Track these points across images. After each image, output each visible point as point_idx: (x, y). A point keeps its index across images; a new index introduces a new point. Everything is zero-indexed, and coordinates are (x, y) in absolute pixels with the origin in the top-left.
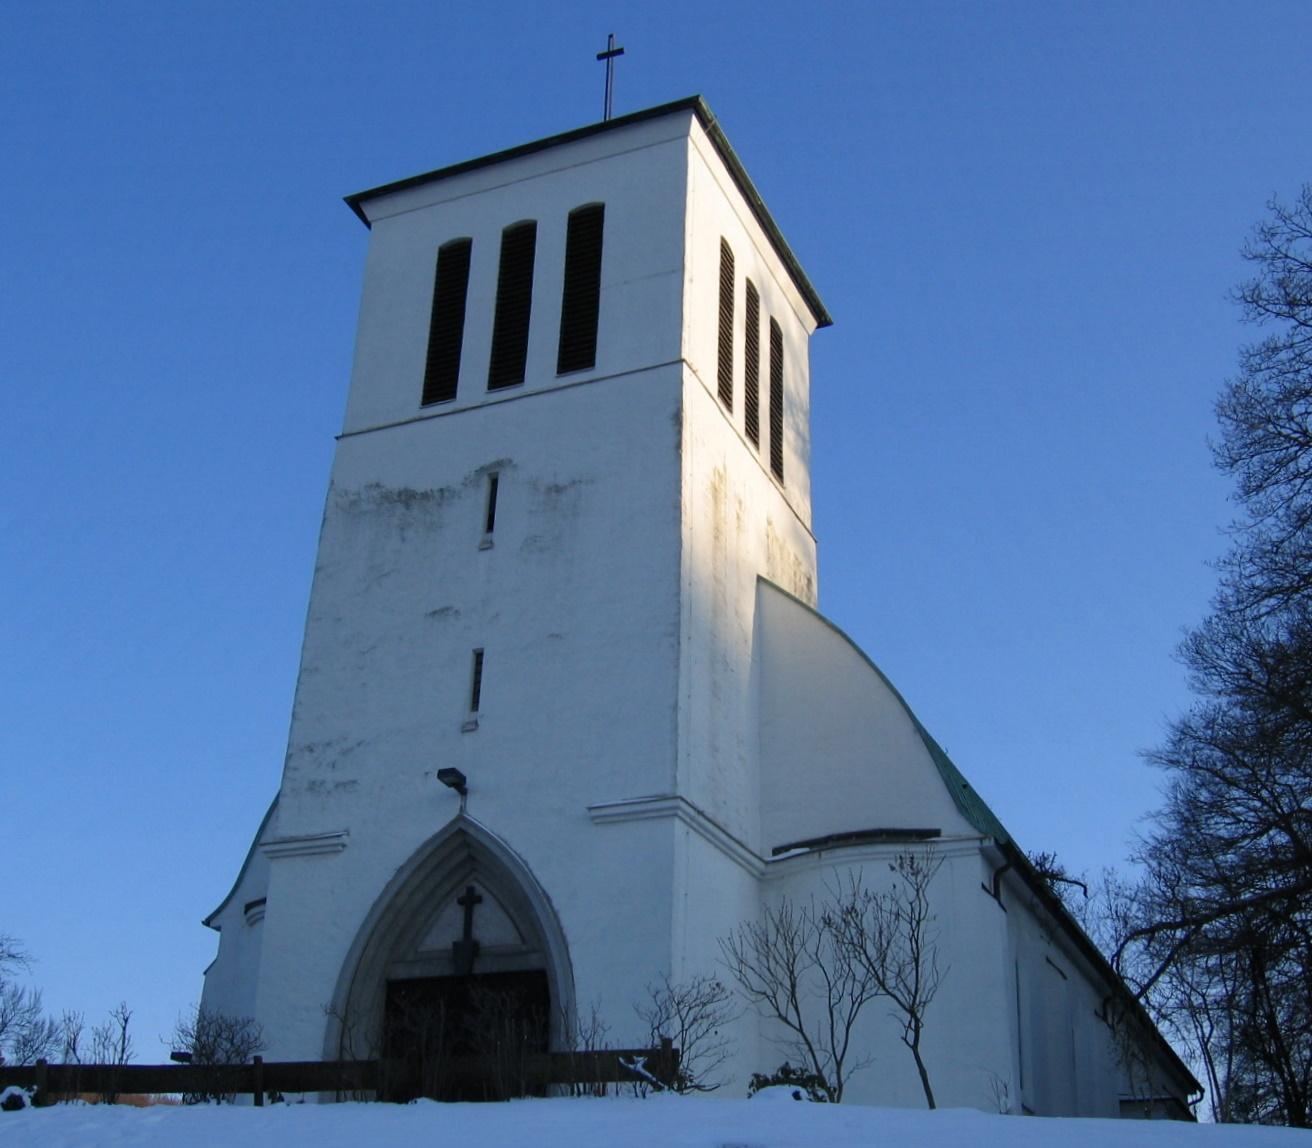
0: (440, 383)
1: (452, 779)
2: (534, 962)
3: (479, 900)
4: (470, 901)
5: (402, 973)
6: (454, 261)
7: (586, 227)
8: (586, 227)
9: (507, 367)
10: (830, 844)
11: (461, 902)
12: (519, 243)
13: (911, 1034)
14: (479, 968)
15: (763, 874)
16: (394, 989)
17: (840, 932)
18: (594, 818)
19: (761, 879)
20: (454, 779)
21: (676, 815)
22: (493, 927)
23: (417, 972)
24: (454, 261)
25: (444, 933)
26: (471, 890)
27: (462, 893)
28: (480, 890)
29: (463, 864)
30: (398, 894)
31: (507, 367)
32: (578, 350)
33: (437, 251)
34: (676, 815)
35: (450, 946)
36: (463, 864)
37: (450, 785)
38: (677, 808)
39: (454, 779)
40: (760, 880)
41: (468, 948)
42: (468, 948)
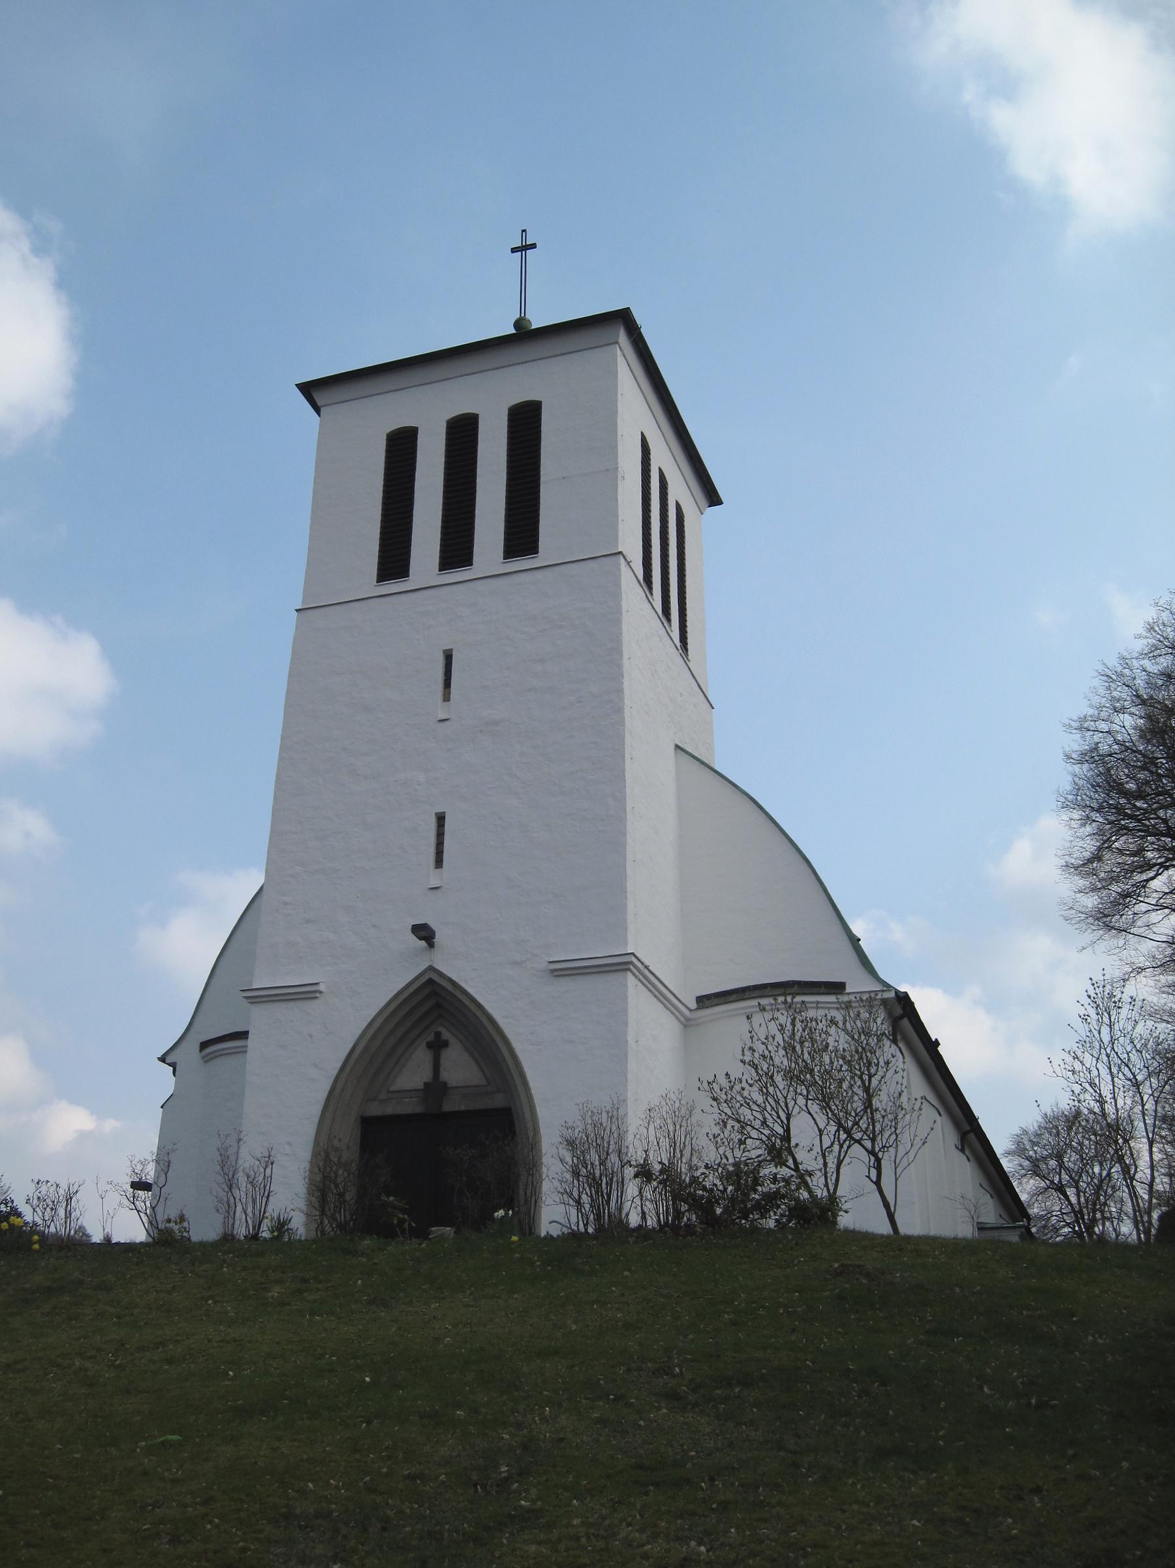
0: (393, 561)
1: (423, 933)
2: (498, 1101)
3: (445, 1044)
4: (437, 1046)
5: (375, 1110)
6: (402, 447)
7: (525, 423)
8: (525, 423)
9: (457, 550)
10: (747, 994)
11: (430, 1046)
12: (462, 433)
13: (874, 1173)
14: (447, 1107)
15: (688, 1020)
16: (373, 1130)
17: (869, 1070)
18: (553, 971)
19: (687, 1024)
20: (424, 933)
21: (629, 970)
22: (459, 1069)
23: (389, 1110)
24: (402, 447)
25: (414, 1074)
26: (438, 1034)
27: (431, 1037)
28: (446, 1035)
29: (433, 1010)
30: (373, 1038)
31: (457, 550)
32: (522, 537)
33: (385, 437)
34: (629, 970)
35: (421, 1086)
36: (433, 1010)
37: (420, 938)
38: (631, 963)
39: (424, 933)
40: (685, 1026)
41: (436, 1088)
42: (436, 1088)
